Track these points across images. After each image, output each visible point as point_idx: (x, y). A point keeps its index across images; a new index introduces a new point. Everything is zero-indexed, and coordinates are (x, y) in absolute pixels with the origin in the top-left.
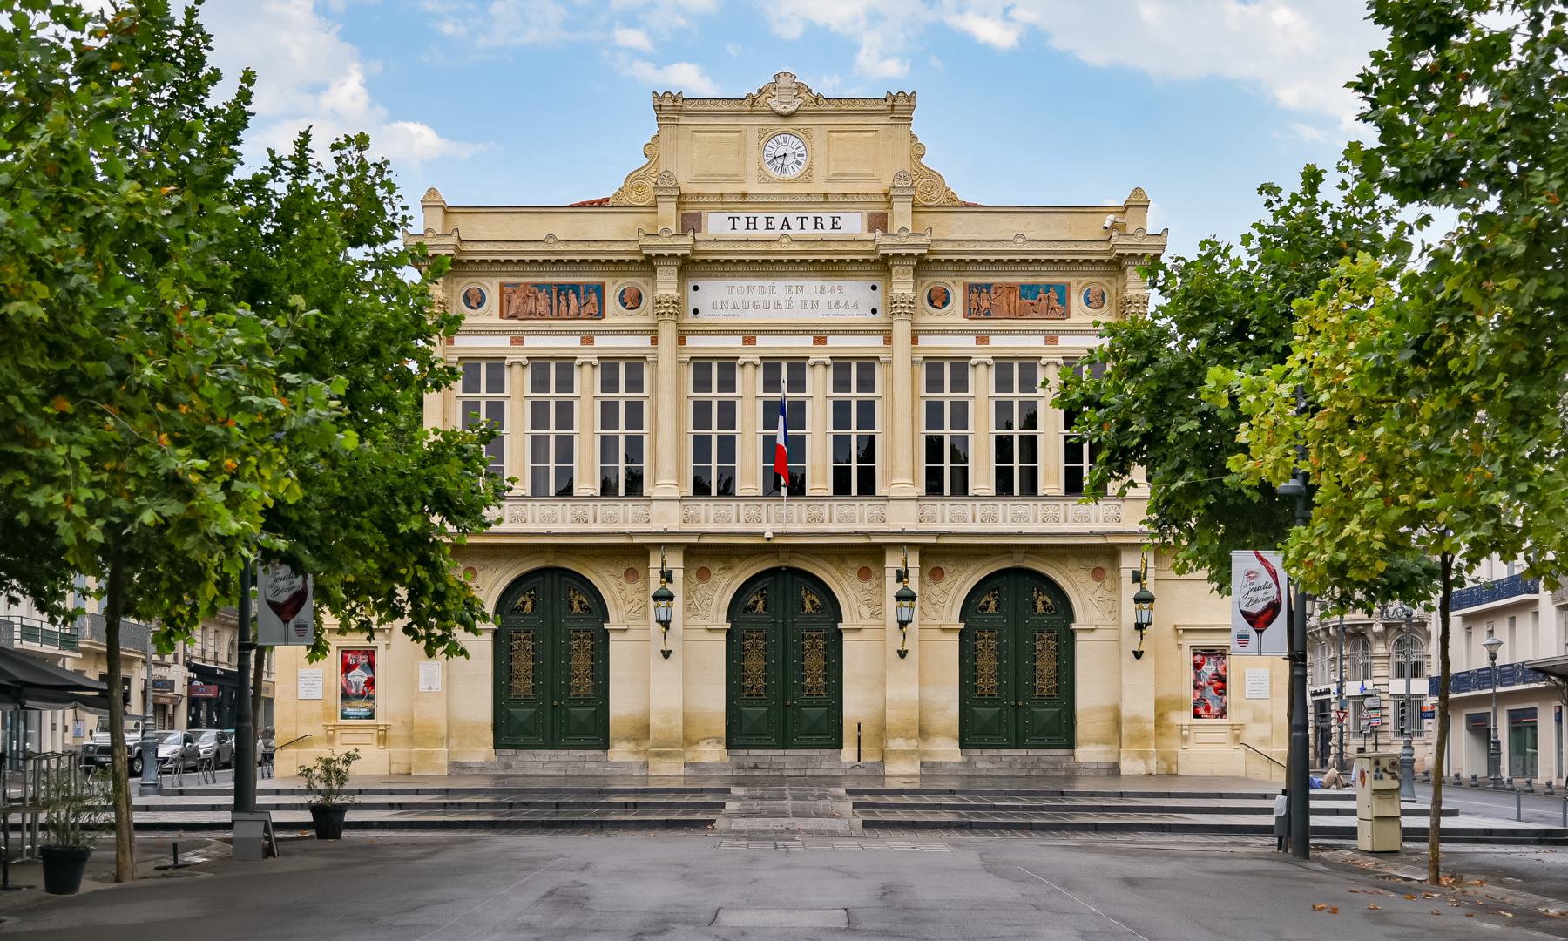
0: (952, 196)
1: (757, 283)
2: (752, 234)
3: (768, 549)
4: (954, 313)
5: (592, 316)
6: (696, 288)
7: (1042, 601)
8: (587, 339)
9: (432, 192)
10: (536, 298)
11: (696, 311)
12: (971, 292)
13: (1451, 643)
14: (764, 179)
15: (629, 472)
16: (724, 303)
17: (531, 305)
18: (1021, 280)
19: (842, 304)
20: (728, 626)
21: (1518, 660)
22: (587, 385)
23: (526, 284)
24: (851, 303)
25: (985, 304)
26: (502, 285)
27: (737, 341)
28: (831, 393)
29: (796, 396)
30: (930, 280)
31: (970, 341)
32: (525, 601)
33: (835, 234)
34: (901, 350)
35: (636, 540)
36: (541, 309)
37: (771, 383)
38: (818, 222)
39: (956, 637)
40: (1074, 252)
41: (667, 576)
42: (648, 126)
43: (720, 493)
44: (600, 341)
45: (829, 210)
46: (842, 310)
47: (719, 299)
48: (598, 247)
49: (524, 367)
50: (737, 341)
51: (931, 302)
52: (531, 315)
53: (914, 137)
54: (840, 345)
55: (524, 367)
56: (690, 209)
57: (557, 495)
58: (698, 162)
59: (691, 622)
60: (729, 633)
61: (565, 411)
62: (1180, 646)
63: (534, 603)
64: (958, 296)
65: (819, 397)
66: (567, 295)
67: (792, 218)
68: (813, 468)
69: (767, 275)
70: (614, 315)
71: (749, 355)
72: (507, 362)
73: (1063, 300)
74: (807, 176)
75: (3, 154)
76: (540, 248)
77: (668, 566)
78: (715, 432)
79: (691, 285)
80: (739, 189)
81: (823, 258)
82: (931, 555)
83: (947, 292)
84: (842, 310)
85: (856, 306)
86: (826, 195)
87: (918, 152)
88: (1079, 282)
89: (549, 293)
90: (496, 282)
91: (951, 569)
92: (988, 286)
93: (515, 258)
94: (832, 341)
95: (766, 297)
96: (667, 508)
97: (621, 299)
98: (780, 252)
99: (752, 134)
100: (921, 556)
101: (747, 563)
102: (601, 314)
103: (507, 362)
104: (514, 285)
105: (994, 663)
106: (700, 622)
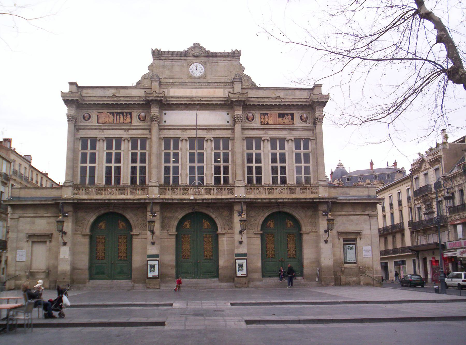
0: (254, 84)
6: (165, 114)
15: (257, 178)
20: (176, 233)
21: (430, 242)
22: (126, 147)
32: (102, 225)
39: (174, 237)
40: (129, 100)
42: (150, 60)
47: (175, 118)
55: (103, 140)
62: (339, 239)
65: (209, 151)
66: (119, 116)
68: (289, 175)
88: (298, 113)
89: (114, 115)
100: (161, 209)
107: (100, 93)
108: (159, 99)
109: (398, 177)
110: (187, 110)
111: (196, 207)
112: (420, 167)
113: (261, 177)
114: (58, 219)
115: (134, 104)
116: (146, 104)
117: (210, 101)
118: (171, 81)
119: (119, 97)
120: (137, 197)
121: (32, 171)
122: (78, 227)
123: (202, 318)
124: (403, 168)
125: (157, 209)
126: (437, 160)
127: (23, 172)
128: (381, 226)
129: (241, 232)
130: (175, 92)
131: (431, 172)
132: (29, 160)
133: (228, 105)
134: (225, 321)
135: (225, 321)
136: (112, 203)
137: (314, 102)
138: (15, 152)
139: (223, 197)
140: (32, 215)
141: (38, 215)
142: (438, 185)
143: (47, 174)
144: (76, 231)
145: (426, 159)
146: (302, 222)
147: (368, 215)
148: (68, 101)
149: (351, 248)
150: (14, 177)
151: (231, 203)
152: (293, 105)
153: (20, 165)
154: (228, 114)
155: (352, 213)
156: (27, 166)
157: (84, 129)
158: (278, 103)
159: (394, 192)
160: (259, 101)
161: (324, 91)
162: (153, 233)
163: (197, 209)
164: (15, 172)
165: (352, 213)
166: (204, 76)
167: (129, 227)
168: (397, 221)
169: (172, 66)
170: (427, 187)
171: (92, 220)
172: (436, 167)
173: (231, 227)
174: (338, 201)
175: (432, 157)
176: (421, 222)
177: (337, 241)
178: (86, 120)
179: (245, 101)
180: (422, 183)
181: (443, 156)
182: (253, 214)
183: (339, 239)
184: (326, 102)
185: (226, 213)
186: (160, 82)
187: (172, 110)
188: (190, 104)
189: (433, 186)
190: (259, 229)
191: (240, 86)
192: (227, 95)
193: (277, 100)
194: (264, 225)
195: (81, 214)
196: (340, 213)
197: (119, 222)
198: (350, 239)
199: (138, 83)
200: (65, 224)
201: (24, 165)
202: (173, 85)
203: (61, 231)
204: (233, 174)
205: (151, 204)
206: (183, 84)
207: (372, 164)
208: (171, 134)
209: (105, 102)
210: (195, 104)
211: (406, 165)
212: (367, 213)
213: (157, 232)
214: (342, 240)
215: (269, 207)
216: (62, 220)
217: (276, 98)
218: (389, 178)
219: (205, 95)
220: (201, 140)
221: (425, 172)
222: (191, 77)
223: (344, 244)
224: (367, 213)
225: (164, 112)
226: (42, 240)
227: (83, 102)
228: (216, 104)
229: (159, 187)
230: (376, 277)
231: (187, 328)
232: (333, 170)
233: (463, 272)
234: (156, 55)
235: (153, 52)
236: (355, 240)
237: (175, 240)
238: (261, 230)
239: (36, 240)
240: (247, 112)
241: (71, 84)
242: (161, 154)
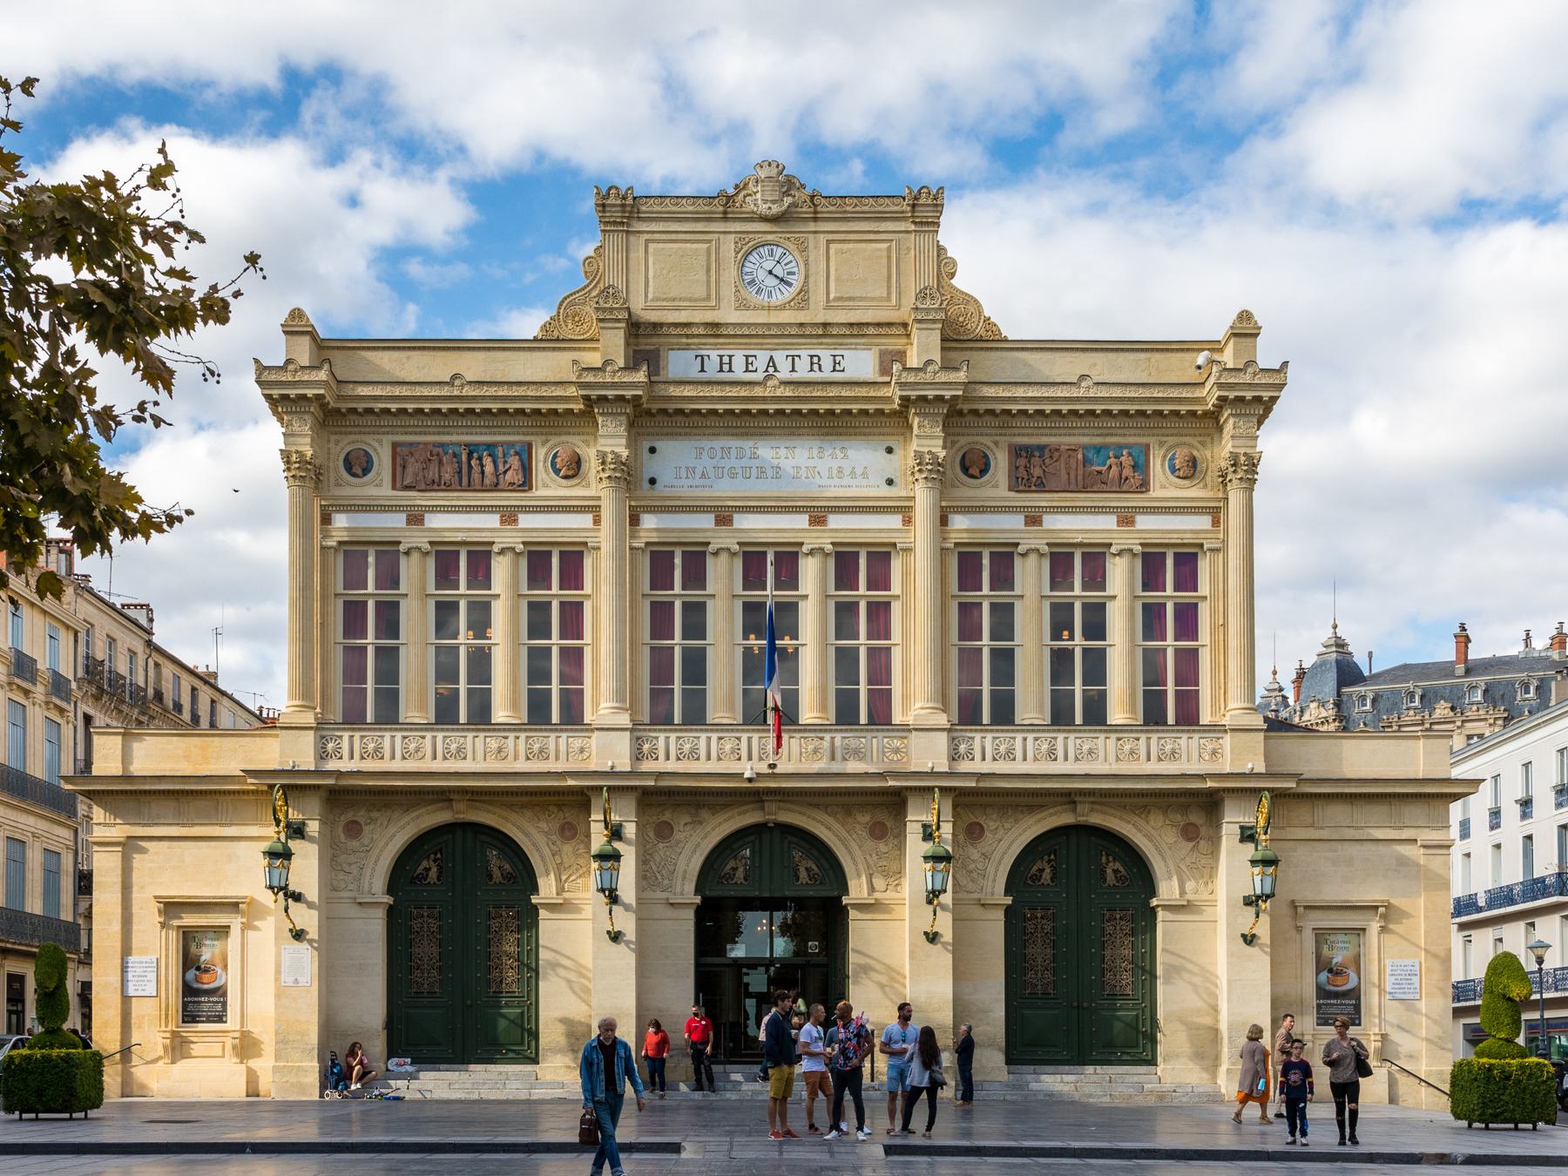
1: (734, 443)
2: (816, 376)
3: (752, 795)
4: (379, 486)
5: (513, 487)
6: (652, 450)
7: (1113, 868)
8: (1126, 519)
9: (297, 314)
10: (440, 462)
11: (653, 481)
12: (1018, 456)
13: (136, 927)
14: (743, 305)
16: (691, 470)
17: (432, 473)
18: (1085, 440)
19: (847, 472)
20: (1009, 900)
23: (426, 444)
24: (859, 471)
25: (1037, 472)
26: (395, 445)
27: (802, 521)
28: (739, 590)
29: (786, 594)
30: (963, 440)
31: (1017, 521)
33: (838, 376)
34: (921, 536)
35: (571, 782)
36: (447, 477)
37: (753, 577)
38: (815, 362)
39: (1000, 915)
41: (616, 833)
43: (872, 721)
44: (526, 521)
45: (828, 346)
46: (847, 480)
48: (520, 391)
49: (1042, 555)
50: (706, 521)
51: (965, 469)
52: (433, 485)
53: (941, 250)
54: (754, 526)
56: (646, 344)
57: (1177, 723)
58: (662, 278)
59: (649, 894)
60: (391, 911)
61: (696, 612)
62: (1299, 929)
63: (440, 868)
64: (1001, 462)
67: (779, 356)
69: (746, 434)
70: (546, 486)
71: (1033, 540)
72: (711, 548)
73: (1141, 467)
74: (802, 299)
75: (1, 269)
76: (445, 391)
77: (615, 818)
78: (464, 639)
79: (646, 445)
80: (709, 317)
81: (822, 407)
82: (970, 806)
83: (986, 456)
84: (847, 480)
85: (864, 475)
86: (825, 325)
87: (945, 266)
90: (388, 440)
91: (992, 825)
92: (1041, 448)
93: (410, 406)
94: (834, 521)
95: (743, 462)
96: (602, 746)
97: (553, 464)
98: (764, 399)
99: (728, 246)
101: (721, 817)
102: (526, 484)
103: (1021, 549)
104: (411, 444)
105: (1049, 951)
106: (660, 895)
113: (838, 681)
116: (582, 413)
121: (157, 665)
122: (341, 876)
127: (122, 668)
132: (143, 622)
138: (90, 591)
143: (215, 675)
146: (1158, 867)
153: (112, 641)
156: (139, 647)
164: (92, 669)
178: (355, 475)
184: (1274, 399)
194: (402, 874)
196: (1301, 833)
197: (1104, 859)
201: (129, 640)
203: (281, 889)
205: (605, 794)
227: (344, 406)
229: (632, 730)
234: (617, 215)
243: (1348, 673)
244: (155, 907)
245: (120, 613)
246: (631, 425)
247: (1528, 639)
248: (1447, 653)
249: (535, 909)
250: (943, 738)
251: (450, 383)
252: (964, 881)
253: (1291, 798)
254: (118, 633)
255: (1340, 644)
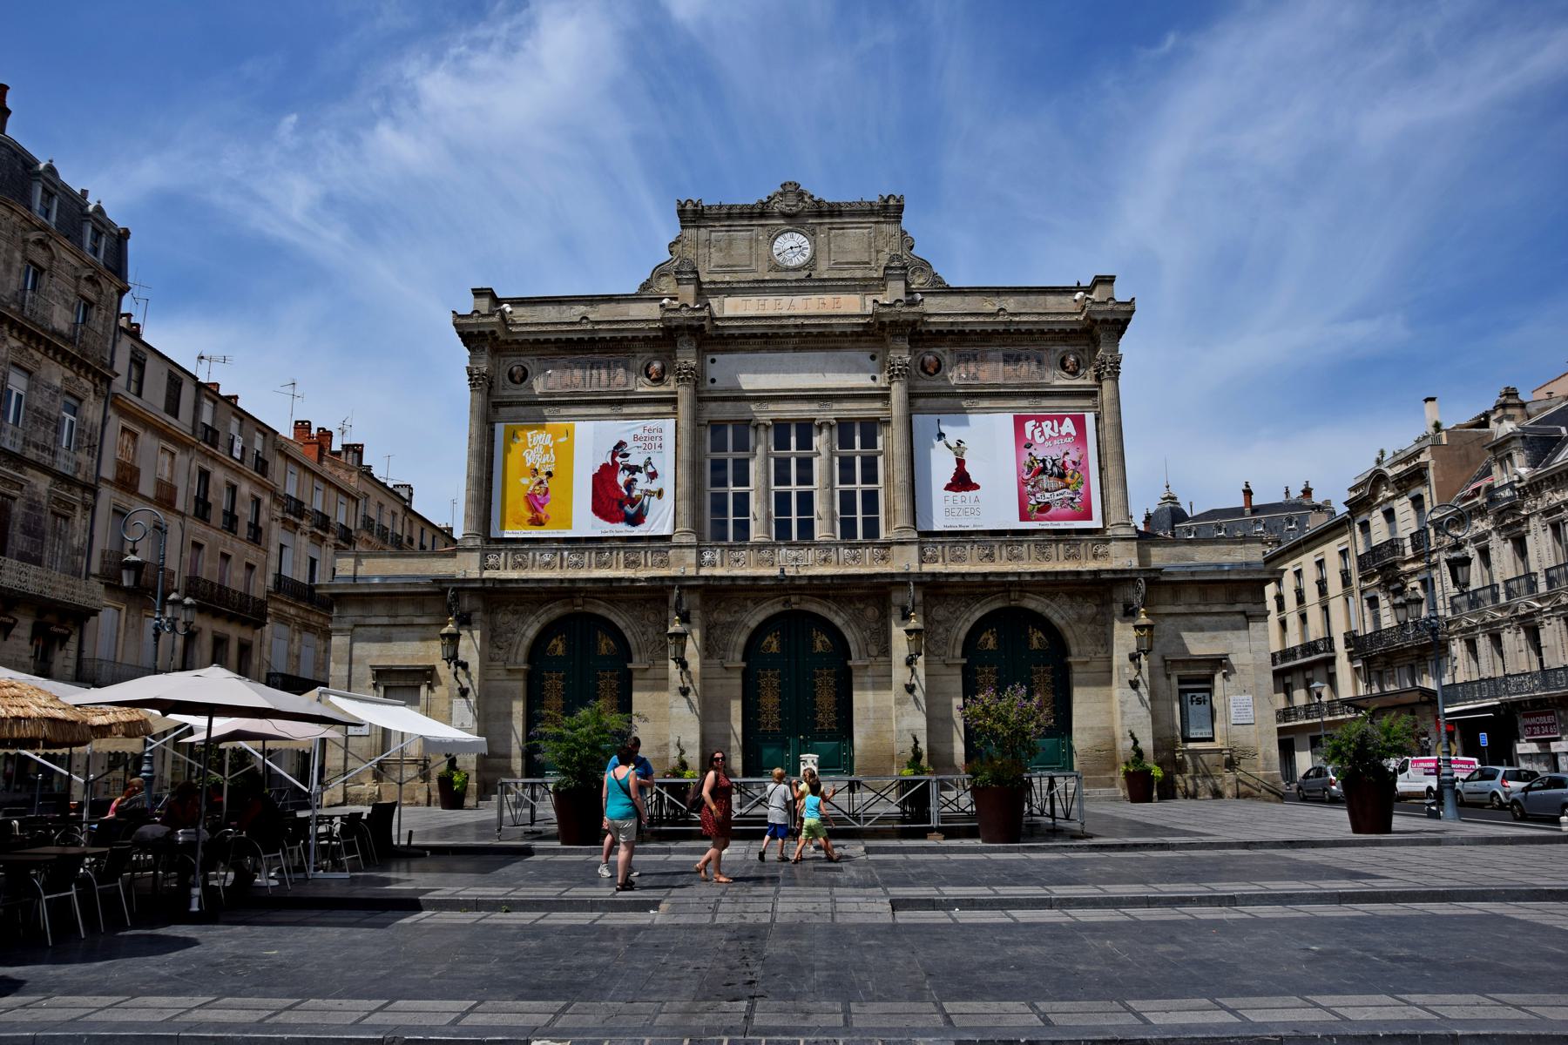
6: (713, 361)
11: (713, 381)
20: (744, 665)
42: (669, 228)
62: (1168, 677)
87: (907, 242)
107: (550, 314)
108: (696, 323)
109: (1316, 522)
110: (769, 351)
111: (793, 599)
112: (1374, 496)
114: (445, 631)
115: (634, 339)
116: (664, 338)
117: (825, 325)
118: (727, 278)
119: (598, 323)
120: (642, 573)
123: (770, 890)
124: (1328, 502)
125: (691, 601)
126: (1417, 475)
127: (387, 523)
128: (1276, 647)
129: (910, 662)
130: (732, 307)
131: (1403, 507)
132: (405, 494)
133: (871, 335)
134: (833, 901)
135: (833, 901)
136: (580, 590)
137: (1095, 321)
139: (863, 571)
140: (385, 621)
141: (400, 620)
142: (1419, 538)
144: (492, 660)
145: (1390, 473)
147: (1243, 613)
148: (471, 336)
149: (1199, 702)
150: (365, 535)
151: (883, 586)
152: (1042, 332)
153: (381, 506)
154: (873, 358)
155: (1201, 608)
156: (399, 510)
157: (510, 404)
158: (1001, 328)
159: (1307, 561)
160: (952, 324)
161: (1121, 293)
162: (683, 664)
163: (797, 603)
164: (368, 523)
165: (1201, 608)
166: (811, 263)
167: (624, 651)
168: (1315, 631)
169: (730, 242)
170: (1393, 545)
171: (531, 632)
172: (1414, 492)
173: (886, 650)
174: (1163, 578)
175: (1403, 467)
176: (1378, 634)
177: (1162, 681)
179: (915, 322)
180: (1380, 532)
181: (1432, 464)
182: (940, 613)
183: (1168, 677)
184: (1128, 321)
185: (871, 612)
186: (699, 283)
187: (731, 351)
188: (776, 335)
189: (1408, 542)
190: (959, 652)
191: (902, 284)
192: (869, 310)
193: (1000, 319)
195: (503, 618)
196: (1169, 609)
198: (1198, 679)
199: (645, 286)
200: (463, 643)
201: (391, 505)
202: (731, 290)
204: (887, 512)
206: (758, 287)
207: (1248, 493)
208: (727, 411)
209: (564, 337)
210: (788, 336)
211: (1335, 494)
212: (1239, 607)
213: (694, 663)
214: (1174, 680)
215: (985, 595)
216: (454, 630)
217: (997, 314)
218: (1291, 526)
219: (812, 311)
220: (806, 430)
221: (1385, 507)
222: (776, 267)
223: (1182, 692)
224: (1239, 607)
225: (709, 357)
226: (410, 683)
227: (510, 339)
228: (844, 334)
230: (1266, 777)
231: (826, 890)
232: (1151, 511)
233: (1501, 764)
235: (682, 212)
236: (1210, 679)
237: (739, 681)
238: (963, 656)
239: (394, 683)
240: (923, 351)
241: (478, 293)
242: (702, 464)
243: (1177, 515)
244: (369, 673)
245: (392, 493)
246: (698, 348)
247: (1287, 493)
248: (1239, 502)
249: (630, 672)
250: (915, 548)
251: (579, 323)
252: (932, 648)
253: (1157, 584)
254: (386, 501)
255: (1172, 498)
